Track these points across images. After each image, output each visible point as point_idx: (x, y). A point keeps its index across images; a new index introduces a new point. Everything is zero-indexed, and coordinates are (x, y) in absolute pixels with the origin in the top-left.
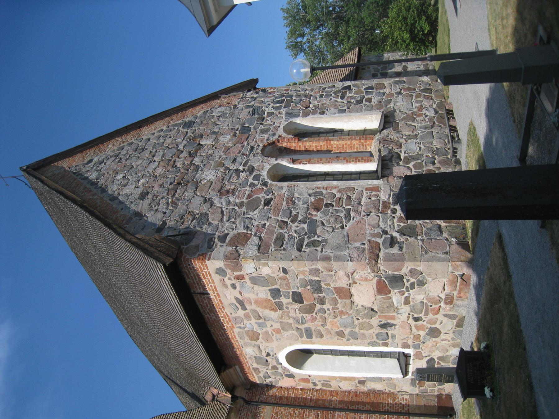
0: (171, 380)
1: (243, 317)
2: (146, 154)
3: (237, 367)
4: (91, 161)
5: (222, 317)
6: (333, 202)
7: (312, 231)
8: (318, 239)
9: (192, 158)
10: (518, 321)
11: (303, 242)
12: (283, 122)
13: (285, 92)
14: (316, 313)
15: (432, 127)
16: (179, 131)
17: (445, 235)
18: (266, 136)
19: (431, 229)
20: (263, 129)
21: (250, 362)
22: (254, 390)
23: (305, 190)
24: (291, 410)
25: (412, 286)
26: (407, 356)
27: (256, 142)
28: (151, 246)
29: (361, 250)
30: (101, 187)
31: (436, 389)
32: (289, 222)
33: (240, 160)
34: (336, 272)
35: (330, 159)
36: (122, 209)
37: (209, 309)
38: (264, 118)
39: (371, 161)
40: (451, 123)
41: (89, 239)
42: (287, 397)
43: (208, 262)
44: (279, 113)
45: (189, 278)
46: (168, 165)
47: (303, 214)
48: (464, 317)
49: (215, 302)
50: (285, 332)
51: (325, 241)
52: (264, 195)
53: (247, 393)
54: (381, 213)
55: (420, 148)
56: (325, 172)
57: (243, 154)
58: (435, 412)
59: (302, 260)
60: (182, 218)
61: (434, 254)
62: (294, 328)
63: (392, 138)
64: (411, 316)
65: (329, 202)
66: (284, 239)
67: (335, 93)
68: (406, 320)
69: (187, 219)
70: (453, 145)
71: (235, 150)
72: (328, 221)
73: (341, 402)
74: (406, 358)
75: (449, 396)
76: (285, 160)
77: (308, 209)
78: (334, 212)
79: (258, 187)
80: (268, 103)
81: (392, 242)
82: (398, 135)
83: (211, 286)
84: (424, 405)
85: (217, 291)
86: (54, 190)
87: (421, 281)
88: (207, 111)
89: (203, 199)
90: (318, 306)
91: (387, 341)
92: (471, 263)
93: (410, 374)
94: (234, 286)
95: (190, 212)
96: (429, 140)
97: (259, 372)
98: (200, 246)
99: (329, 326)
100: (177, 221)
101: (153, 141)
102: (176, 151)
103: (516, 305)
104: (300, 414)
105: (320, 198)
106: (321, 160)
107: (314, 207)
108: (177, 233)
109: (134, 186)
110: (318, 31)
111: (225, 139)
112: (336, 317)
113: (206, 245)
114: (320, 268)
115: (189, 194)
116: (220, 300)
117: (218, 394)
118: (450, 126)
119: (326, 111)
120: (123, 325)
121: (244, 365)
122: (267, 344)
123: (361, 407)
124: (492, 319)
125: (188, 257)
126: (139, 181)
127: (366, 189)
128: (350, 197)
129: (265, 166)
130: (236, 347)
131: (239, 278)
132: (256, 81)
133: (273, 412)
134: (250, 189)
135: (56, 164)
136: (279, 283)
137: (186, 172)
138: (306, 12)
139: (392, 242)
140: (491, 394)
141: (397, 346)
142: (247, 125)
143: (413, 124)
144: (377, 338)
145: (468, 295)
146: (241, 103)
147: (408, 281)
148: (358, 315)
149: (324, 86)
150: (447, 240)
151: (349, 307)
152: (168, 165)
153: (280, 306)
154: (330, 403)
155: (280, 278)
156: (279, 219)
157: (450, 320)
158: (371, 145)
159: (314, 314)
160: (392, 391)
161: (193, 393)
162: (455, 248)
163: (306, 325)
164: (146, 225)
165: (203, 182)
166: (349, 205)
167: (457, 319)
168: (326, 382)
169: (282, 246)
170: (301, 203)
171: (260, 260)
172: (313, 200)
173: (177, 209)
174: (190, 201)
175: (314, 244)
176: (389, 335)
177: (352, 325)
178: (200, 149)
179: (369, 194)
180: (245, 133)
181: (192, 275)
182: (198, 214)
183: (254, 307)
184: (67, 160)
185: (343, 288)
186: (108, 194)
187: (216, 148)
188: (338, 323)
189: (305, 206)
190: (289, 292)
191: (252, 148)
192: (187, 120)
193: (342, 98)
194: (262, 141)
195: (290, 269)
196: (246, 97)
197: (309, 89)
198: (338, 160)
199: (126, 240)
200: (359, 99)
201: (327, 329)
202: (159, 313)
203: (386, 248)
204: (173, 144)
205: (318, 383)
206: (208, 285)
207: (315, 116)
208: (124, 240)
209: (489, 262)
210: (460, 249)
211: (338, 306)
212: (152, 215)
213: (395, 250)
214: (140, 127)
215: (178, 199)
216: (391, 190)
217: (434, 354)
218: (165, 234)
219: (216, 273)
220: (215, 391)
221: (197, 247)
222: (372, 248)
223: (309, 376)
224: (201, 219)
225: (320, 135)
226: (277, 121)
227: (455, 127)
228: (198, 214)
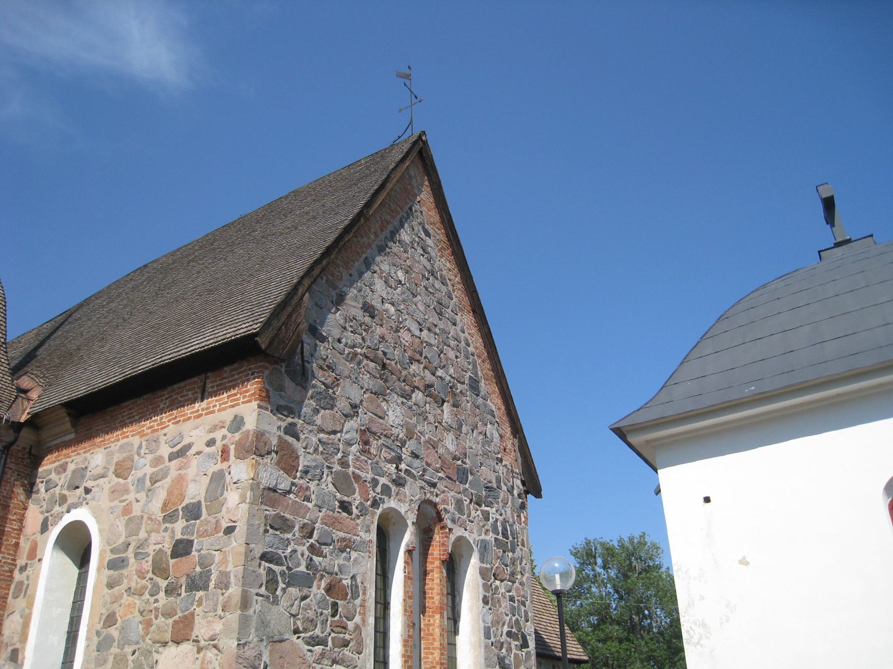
0: (63, 322)
1: (157, 454)
2: (433, 319)
3: (72, 436)
4: (428, 234)
6: (340, 617)
7: (293, 580)
8: (279, 589)
9: (422, 389)
11: (277, 564)
12: (472, 537)
13: (520, 540)
14: (152, 579)
18: (451, 508)
22: (29, 461)
23: (362, 570)
27: (443, 492)
28: (289, 316)
30: (387, 246)
32: (311, 541)
33: (415, 465)
36: (351, 275)
37: (177, 399)
38: (480, 505)
41: (308, 220)
42: (7, 518)
43: (255, 404)
44: (487, 530)
45: (231, 371)
46: (415, 351)
49: (188, 410)
50: (124, 522)
51: (276, 602)
52: (357, 502)
53: (24, 448)
56: (389, 603)
57: (424, 470)
59: (246, 561)
62: (130, 539)
65: (340, 609)
66: (284, 531)
67: (517, 621)
71: (431, 457)
72: (309, 607)
76: (413, 537)
77: (330, 574)
78: (323, 617)
79: (371, 492)
80: (503, 512)
83: (214, 406)
85: (207, 414)
86: (389, 176)
88: (494, 416)
89: (358, 402)
90: (163, 583)
94: (211, 443)
95: (338, 380)
97: (59, 473)
98: (283, 393)
99: (126, 599)
100: (325, 360)
101: (452, 331)
102: (435, 364)
106: (410, 598)
108: (306, 359)
109: (385, 296)
110: (611, 590)
111: (449, 442)
112: (141, 613)
113: (282, 403)
114: (230, 590)
116: (189, 418)
117: (29, 400)
119: (488, 607)
120: (165, 256)
121: (73, 448)
122: (106, 492)
125: (267, 372)
126: (393, 304)
128: (347, 646)
129: (403, 504)
130: (107, 437)
131: (225, 453)
132: (538, 494)
134: (369, 480)
135: (427, 183)
136: (210, 518)
137: (402, 379)
138: (640, 573)
142: (470, 478)
146: (505, 470)
148: (142, 654)
149: (527, 603)
151: (157, 638)
152: (415, 351)
155: (217, 522)
156: (317, 525)
159: (150, 575)
163: (132, 560)
164: (322, 310)
165: (383, 404)
168: (25, 590)
169: (272, 527)
170: (342, 562)
171: (252, 489)
172: (344, 582)
173: (344, 361)
174: (356, 381)
175: (272, 583)
180: (458, 474)
181: (236, 377)
183: (173, 473)
184: (432, 200)
185: (192, 630)
186: (375, 257)
187: (436, 427)
188: (131, 616)
189: (336, 569)
190: (193, 534)
191: (434, 485)
192: (482, 384)
193: (509, 634)
194: (444, 501)
195: (233, 539)
196: (513, 477)
197: (524, 579)
198: (408, 626)
199: (302, 278)
200: (507, 662)
201: (121, 597)
204: (447, 359)
205: (25, 574)
206: (217, 401)
207: (481, 589)
208: (302, 274)
211: (161, 619)
212: (337, 321)
214: (474, 311)
215: (359, 363)
218: (306, 338)
219: (236, 416)
220: (34, 395)
221: (280, 389)
223: (40, 560)
226: (474, 526)
228: (334, 393)
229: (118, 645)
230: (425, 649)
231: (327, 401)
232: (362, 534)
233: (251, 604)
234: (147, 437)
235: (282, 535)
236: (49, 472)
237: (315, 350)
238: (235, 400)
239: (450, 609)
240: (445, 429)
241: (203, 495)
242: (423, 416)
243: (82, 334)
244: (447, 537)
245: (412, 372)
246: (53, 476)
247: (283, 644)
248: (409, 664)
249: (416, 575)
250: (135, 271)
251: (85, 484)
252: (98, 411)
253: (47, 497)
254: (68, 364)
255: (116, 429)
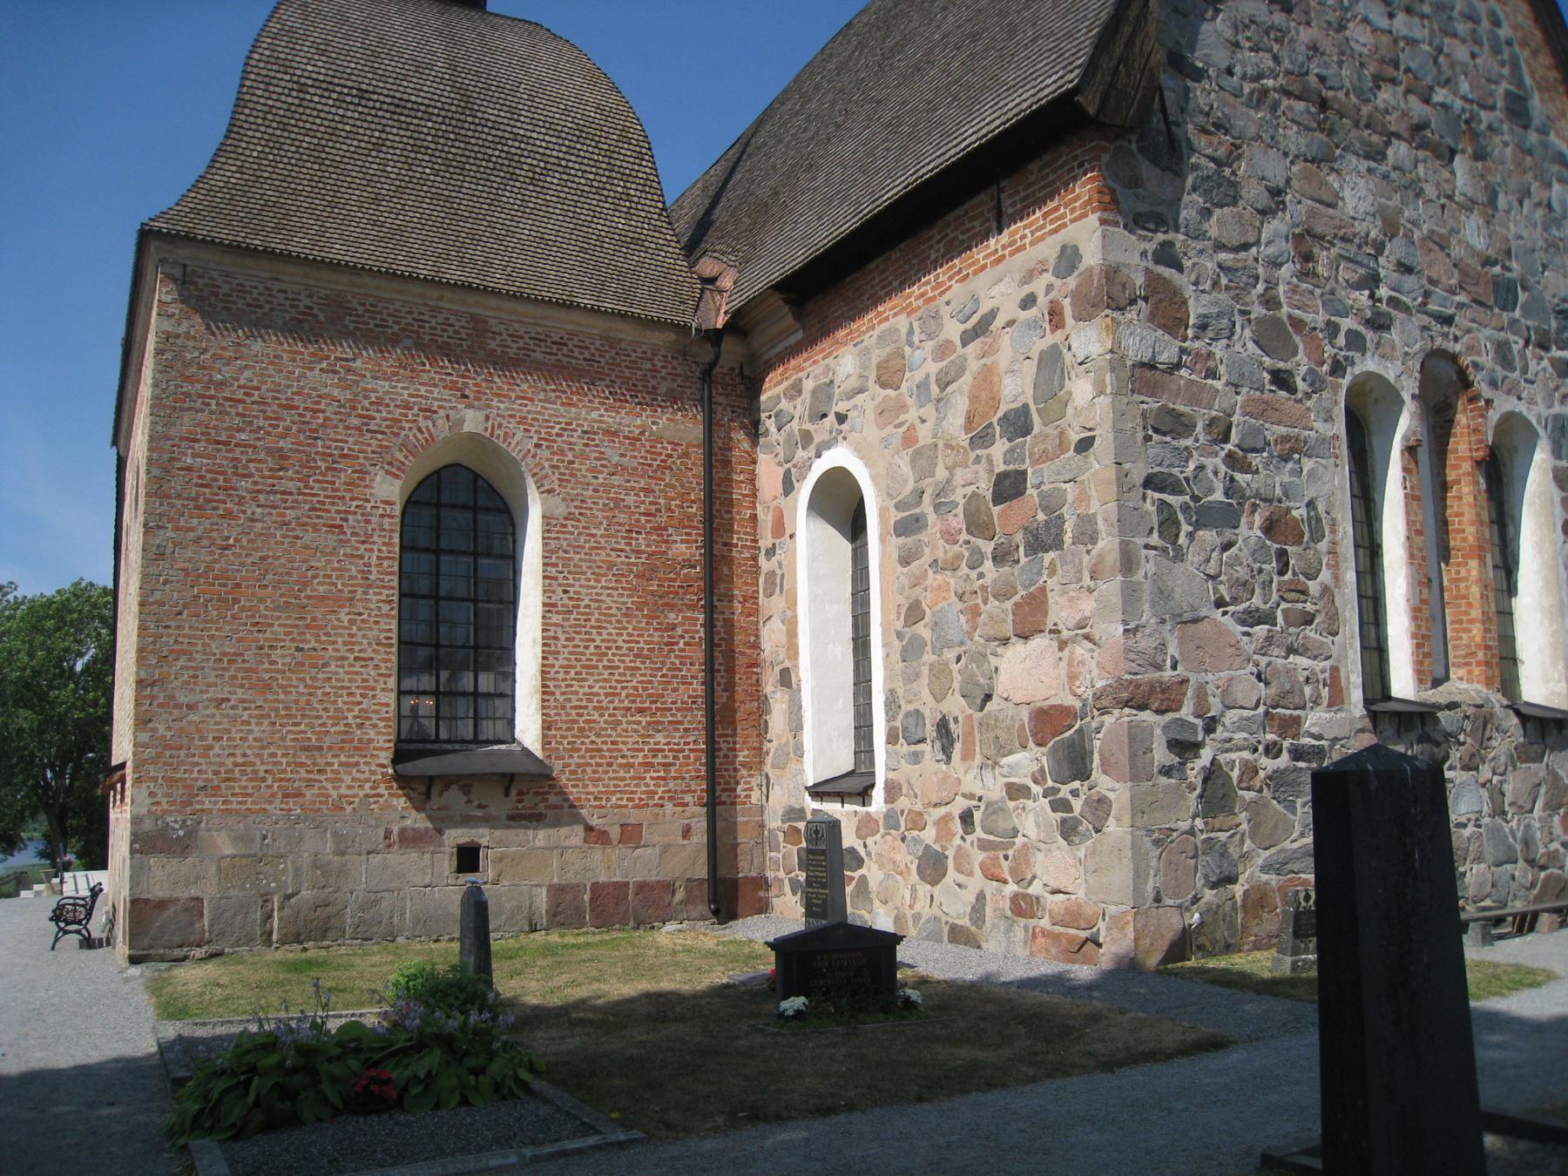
1: (942, 337)
5: (937, 277)
6: (1294, 574)
7: (1205, 517)
8: (1182, 535)
9: (1406, 135)
10: (991, 1085)
11: (1173, 493)
12: (1535, 410)
14: (968, 542)
15: (1531, 862)
16: (1496, 83)
17: (1209, 895)
18: (1487, 360)
19: (1224, 854)
20: (1510, 349)
21: (817, 370)
23: (1325, 490)
24: (697, 494)
25: (1061, 805)
26: (864, 795)
27: (1469, 331)
28: (1129, 44)
29: (1159, 659)
31: (781, 874)
32: (1228, 447)
34: (1090, 591)
35: (1423, 559)
37: (956, 238)
38: (1546, 349)
39: (1420, 681)
40: (1545, 918)
42: (731, 480)
43: (1093, 219)
45: (1041, 169)
46: (1382, 61)
47: (1254, 486)
48: (979, 947)
49: (979, 254)
51: (1179, 556)
52: (1303, 369)
53: (732, 369)
54: (1267, 713)
55: (1465, 826)
56: (1380, 546)
57: (1427, 294)
58: (723, 872)
59: (1120, 492)
60: (1217, 126)
61: (1154, 863)
63: (1494, 743)
64: (975, 803)
65: (1292, 562)
68: (965, 789)
69: (1216, 141)
70: (1476, 920)
71: (1438, 267)
73: (729, 623)
74: (859, 794)
75: (763, 907)
76: (1416, 423)
78: (1263, 577)
81: (1184, 747)
82: (1503, 759)
83: (1023, 237)
84: (737, 845)
85: (1012, 254)
87: (1074, 829)
89: (1282, 183)
90: (988, 547)
91: (902, 740)
92: (1129, 968)
93: (816, 805)
94: (1028, 302)
95: (1238, 147)
96: (1490, 853)
97: (791, 398)
98: (1140, 191)
99: (933, 579)
100: (1207, 114)
102: (1428, 80)
103: (1033, 1080)
104: (690, 517)
105: (1302, 535)
106: (1419, 533)
107: (1275, 517)
108: (1172, 119)
111: (1473, 234)
112: (960, 597)
113: (1142, 208)
114: (1100, 544)
115: (1293, 138)
116: (984, 267)
117: (721, 292)
118: (1535, 916)
121: (805, 355)
123: (720, 678)
124: (984, 1019)
125: (1105, 157)
127: (1335, 670)
129: (1394, 364)
130: (854, 326)
131: (1055, 314)
133: (689, 445)
134: (1320, 325)
136: (1048, 430)
137: (1363, 123)
139: (1184, 747)
140: (790, 1013)
141: (889, 769)
143: (1539, 804)
144: (908, 715)
145: (1040, 958)
147: (1075, 793)
148: (972, 659)
150: (1196, 900)
151: (991, 633)
153: (981, 439)
154: (726, 595)
156: (1235, 419)
157: (969, 910)
158: (1470, 681)
159: (964, 536)
160: (769, 759)
161: (711, 223)
162: (1172, 923)
165: (1332, 178)
166: (1286, 620)
167: (973, 928)
168: (780, 583)
169: (1156, 431)
170: (1287, 479)
171: (1113, 370)
172: (1295, 513)
173: (1244, 109)
174: (1273, 144)
175: (1168, 524)
176: (920, 747)
177: (942, 644)
178: (1438, 157)
179: (1321, 677)
180: (1496, 292)
181: (1051, 178)
182: (1234, 173)
183: (974, 366)
185: (1046, 614)
187: (1443, 207)
188: (945, 604)
189: (1278, 491)
190: (1023, 461)
191: (1448, 320)
192: (1536, 103)
194: (1471, 349)
195: (1092, 459)
198: (1420, 583)
202: (930, 96)
203: (1165, 728)
204: (1452, 66)
206: (1025, 227)
209: (1141, 1015)
210: (1170, 936)
211: (993, 603)
212: (1219, 34)
213: (1161, 755)
215: (1274, 107)
216: (1335, 740)
217: (874, 866)
218: (1168, 81)
219: (1064, 248)
220: (726, 282)
221: (1135, 183)
222: (1163, 691)
223: (792, 536)
224: (1220, 186)
225: (1495, 527)
226: (1537, 391)
227: (1531, 929)
228: (1234, 173)
229: (933, 649)
230: (1452, 622)
231: (1224, 192)
232: (1318, 425)
233: (1138, 563)
234: (919, 313)
235: (1175, 443)
236: (777, 399)
237: (1187, 99)
238: (1058, 219)
239: (1497, 550)
240: (1461, 207)
241: (1030, 392)
242: (1414, 189)
243: (774, 167)
244: (1482, 416)
245: (1382, 106)
246: (784, 404)
247: (1199, 625)
248: (1426, 650)
249: (1426, 490)
250: (834, 39)
251: (836, 409)
252: (828, 288)
253: (781, 439)
254: (765, 223)
255: (866, 310)
